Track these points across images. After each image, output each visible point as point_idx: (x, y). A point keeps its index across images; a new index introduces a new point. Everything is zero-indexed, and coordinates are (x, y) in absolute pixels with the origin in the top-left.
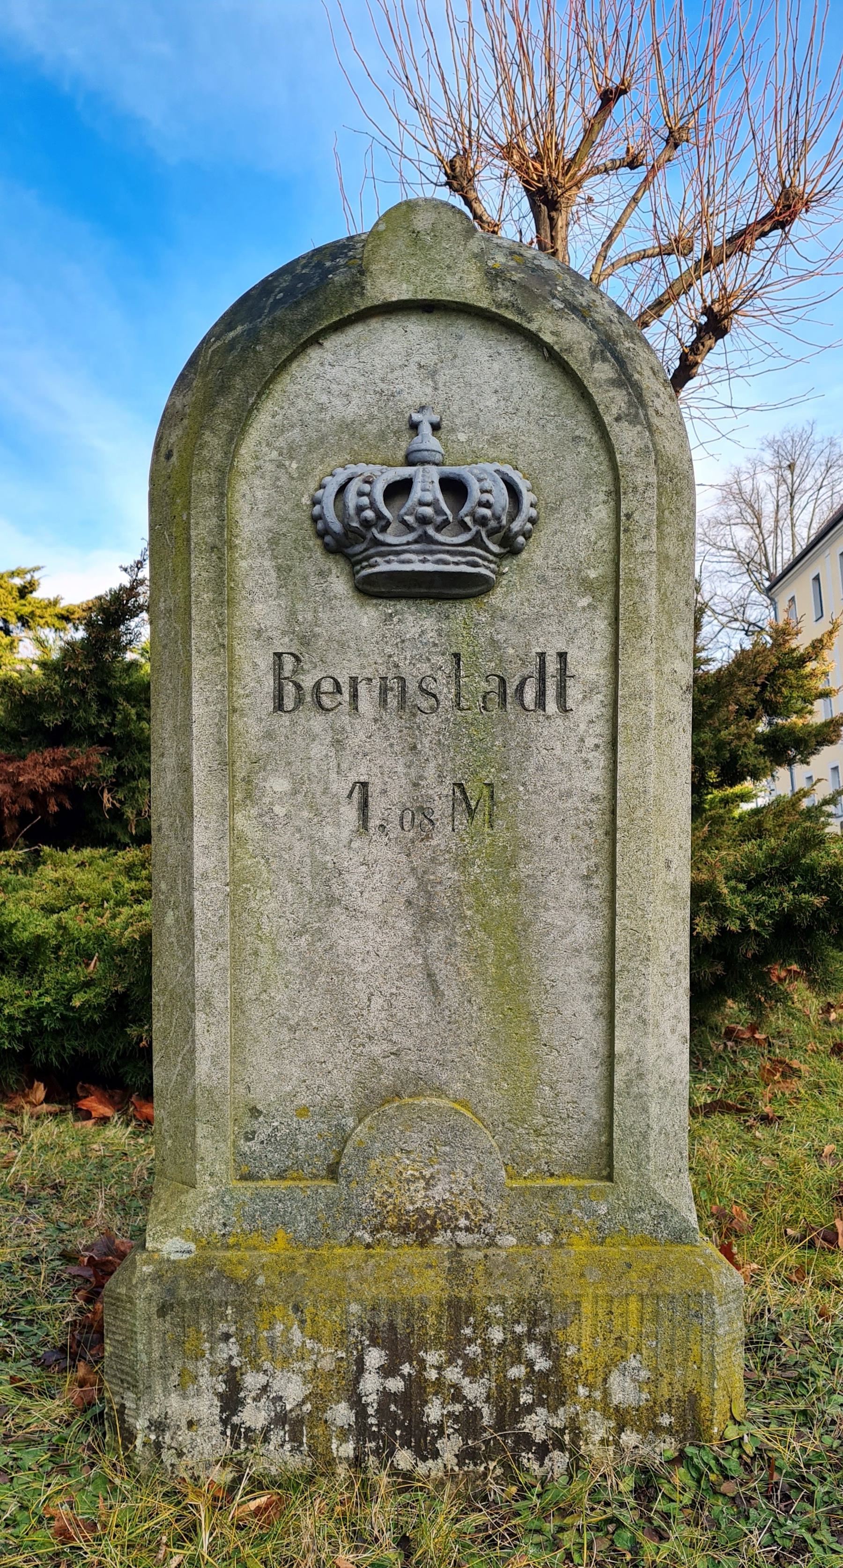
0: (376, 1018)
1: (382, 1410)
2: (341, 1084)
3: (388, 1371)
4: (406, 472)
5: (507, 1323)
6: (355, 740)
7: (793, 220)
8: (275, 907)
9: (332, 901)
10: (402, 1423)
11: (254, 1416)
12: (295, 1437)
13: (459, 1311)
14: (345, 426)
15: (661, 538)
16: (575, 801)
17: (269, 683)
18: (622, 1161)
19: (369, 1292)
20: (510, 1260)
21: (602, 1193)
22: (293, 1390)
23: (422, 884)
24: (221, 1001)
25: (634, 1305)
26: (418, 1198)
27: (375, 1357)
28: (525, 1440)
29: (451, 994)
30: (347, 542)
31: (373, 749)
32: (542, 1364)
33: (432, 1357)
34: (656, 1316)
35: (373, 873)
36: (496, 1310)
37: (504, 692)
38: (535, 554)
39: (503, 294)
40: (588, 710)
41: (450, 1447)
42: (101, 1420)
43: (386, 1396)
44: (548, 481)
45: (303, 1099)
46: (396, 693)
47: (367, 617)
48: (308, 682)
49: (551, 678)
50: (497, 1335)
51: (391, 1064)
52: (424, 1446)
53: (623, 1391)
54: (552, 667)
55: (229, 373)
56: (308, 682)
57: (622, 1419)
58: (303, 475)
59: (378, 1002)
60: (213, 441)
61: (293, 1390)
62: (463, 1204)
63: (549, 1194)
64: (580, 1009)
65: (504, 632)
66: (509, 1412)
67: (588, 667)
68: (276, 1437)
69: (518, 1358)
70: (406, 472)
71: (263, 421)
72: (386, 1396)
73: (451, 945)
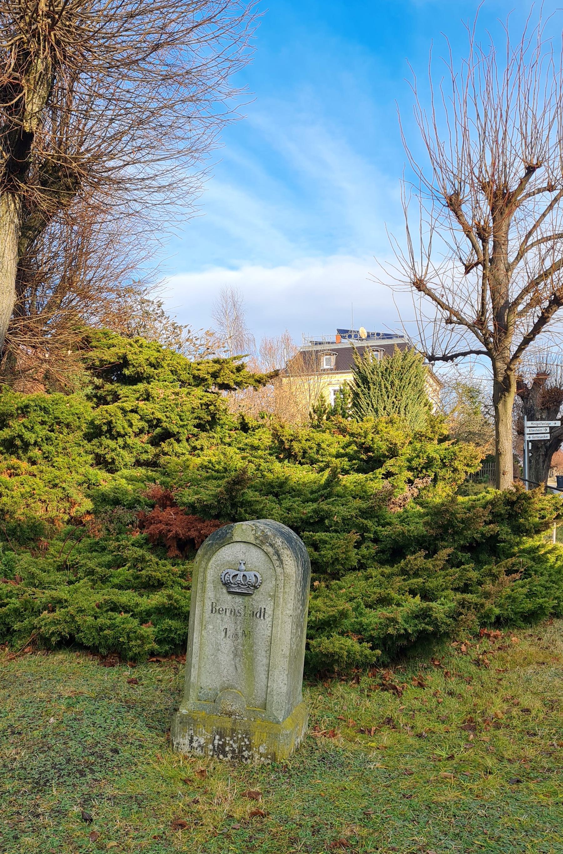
0: (225, 673)
1: (218, 747)
2: (218, 685)
3: (219, 740)
4: (237, 572)
5: (242, 734)
6: (225, 620)
7: (392, 458)
8: (208, 650)
9: (219, 650)
10: (221, 750)
11: (195, 744)
12: (202, 750)
13: (233, 730)
14: (228, 561)
15: (284, 589)
16: (265, 636)
17: (210, 608)
18: (268, 707)
19: (217, 725)
20: (244, 723)
21: (264, 713)
22: (202, 741)
23: (235, 649)
24: (197, 667)
25: (265, 734)
26: (229, 709)
27: (217, 737)
28: (243, 756)
29: (239, 670)
30: (226, 584)
31: (227, 622)
32: (247, 743)
33: (228, 739)
34: (269, 737)
35: (227, 645)
36: (240, 731)
37: (253, 614)
38: (261, 589)
39: (258, 542)
40: (268, 619)
41: (229, 756)
42: (169, 742)
43: (219, 744)
44: (264, 576)
45: (210, 687)
46: (234, 612)
47: (229, 597)
48: (217, 608)
49: (262, 613)
50: (240, 736)
51: (227, 682)
52: (225, 754)
53: (262, 750)
54: (263, 610)
55: (207, 551)
56: (217, 608)
57: (261, 755)
58: (220, 570)
59: (226, 670)
60: (203, 563)
61: (202, 741)
62: (238, 711)
63: (254, 711)
64: (263, 676)
65: (254, 603)
66: (241, 751)
67: (269, 612)
68: (199, 749)
69: (243, 741)
70: (237, 572)
71: (213, 559)
72: (219, 744)
73: (240, 661)
